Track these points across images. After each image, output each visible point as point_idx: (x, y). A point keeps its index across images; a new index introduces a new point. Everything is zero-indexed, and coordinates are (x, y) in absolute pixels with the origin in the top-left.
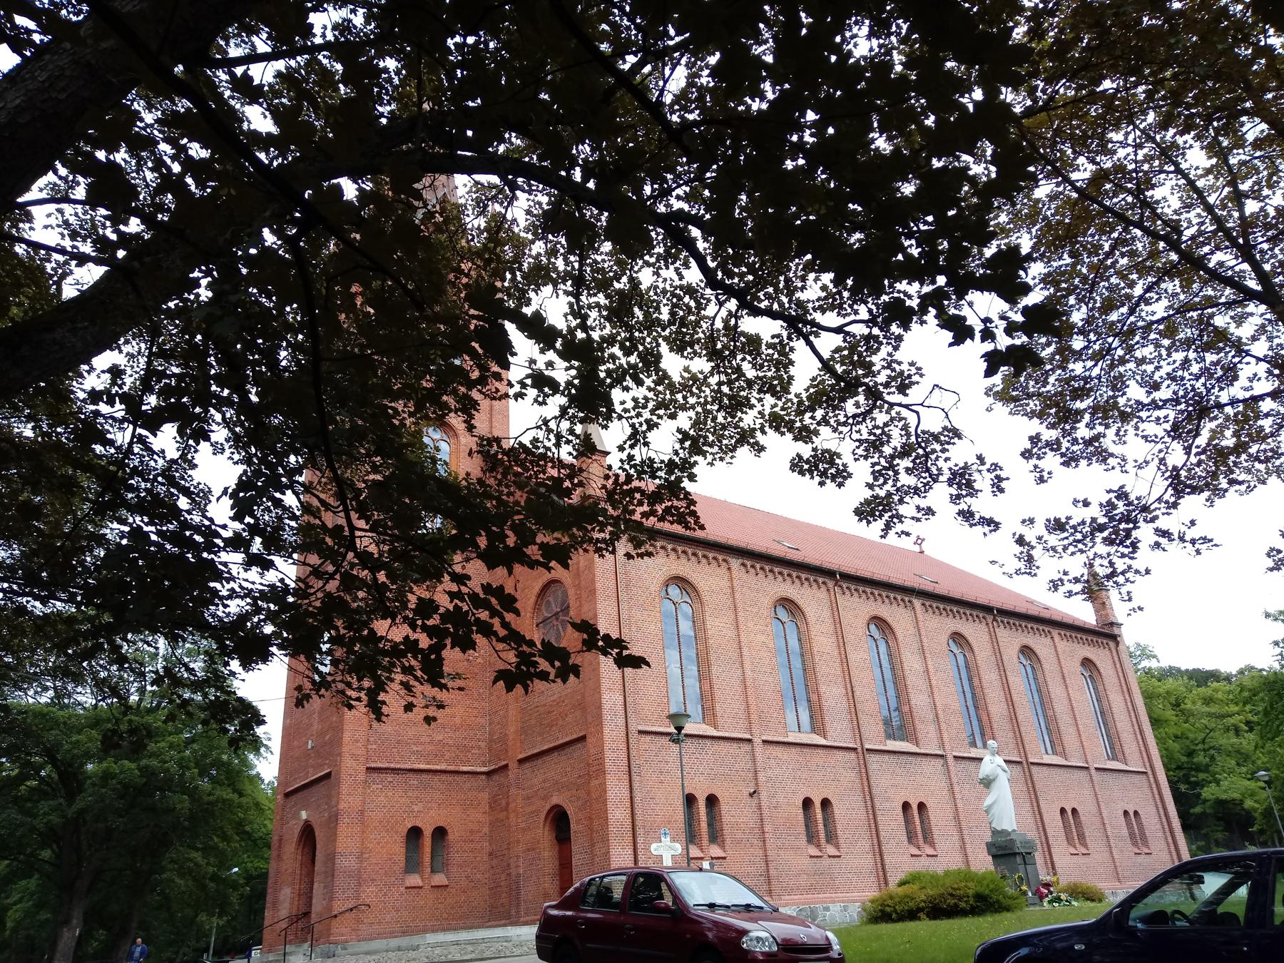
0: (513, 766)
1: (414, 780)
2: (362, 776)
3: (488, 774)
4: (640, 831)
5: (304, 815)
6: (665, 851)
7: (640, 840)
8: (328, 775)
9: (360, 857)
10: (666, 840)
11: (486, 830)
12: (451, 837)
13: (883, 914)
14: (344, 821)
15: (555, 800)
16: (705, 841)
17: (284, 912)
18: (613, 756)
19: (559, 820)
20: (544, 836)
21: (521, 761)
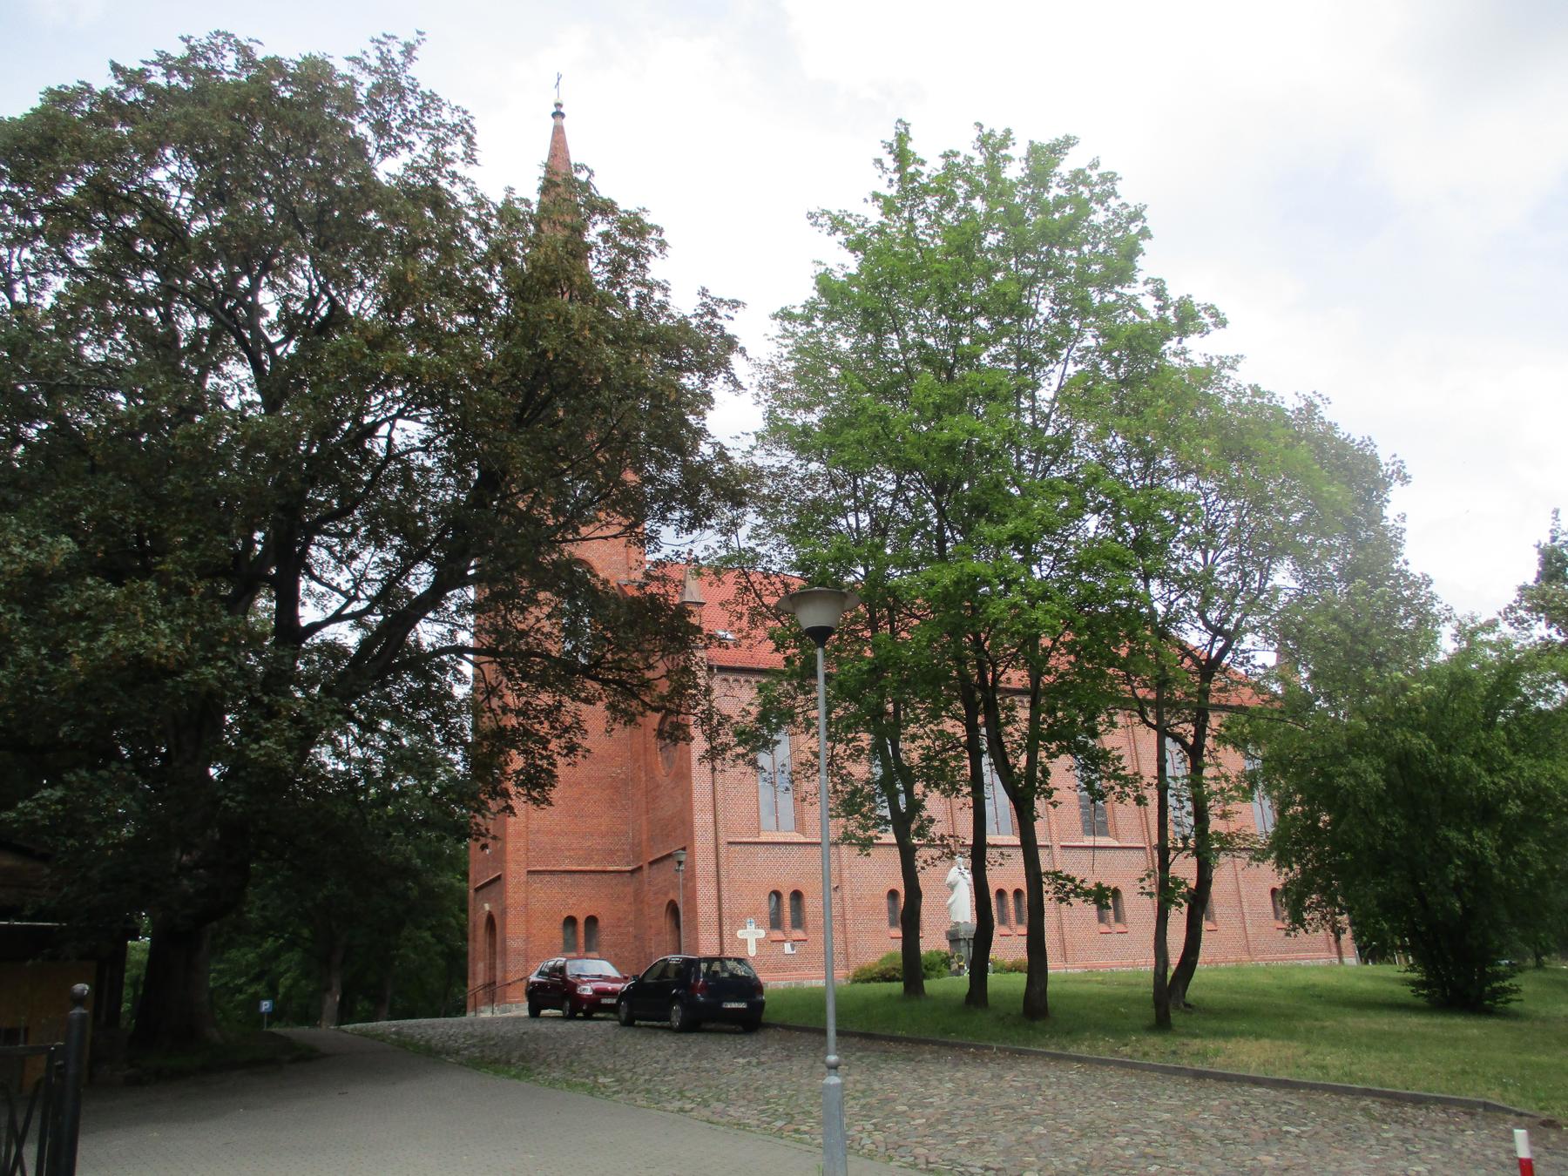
0: (646, 867)
1: (568, 879)
2: (524, 878)
3: (632, 872)
4: (725, 921)
5: (487, 907)
6: (751, 938)
7: (726, 928)
8: (499, 877)
9: (527, 940)
10: (751, 928)
11: (631, 917)
12: (601, 924)
13: (857, 979)
14: (511, 913)
15: (671, 896)
16: (788, 928)
17: (480, 981)
18: (703, 862)
19: (673, 909)
20: (664, 922)
21: (651, 863)
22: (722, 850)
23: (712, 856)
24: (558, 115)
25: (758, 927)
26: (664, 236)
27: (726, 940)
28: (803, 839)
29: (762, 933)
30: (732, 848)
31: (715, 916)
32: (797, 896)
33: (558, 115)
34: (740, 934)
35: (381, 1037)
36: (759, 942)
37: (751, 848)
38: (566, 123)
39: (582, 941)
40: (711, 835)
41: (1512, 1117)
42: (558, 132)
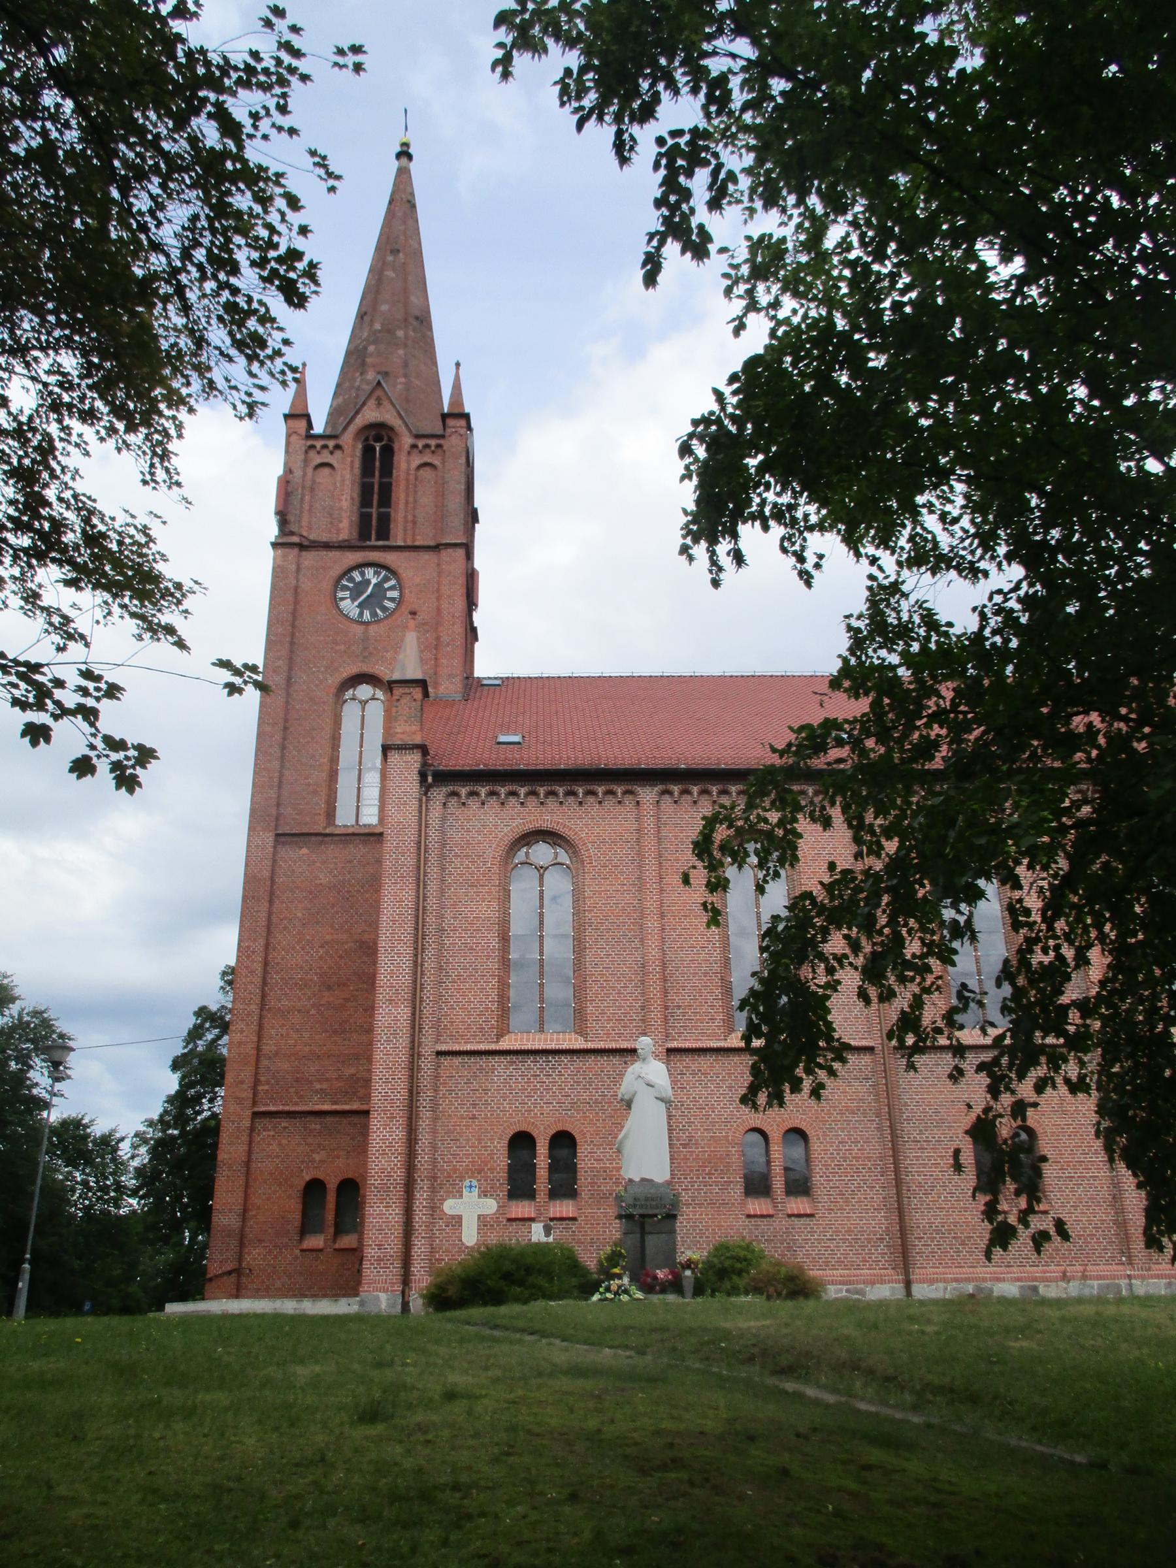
1: (315, 1125)
7: (421, 1197)
16: (542, 1196)
22: (427, 1065)
23: (402, 1075)
24: (404, 154)
25: (484, 1194)
26: (722, 576)
27: (420, 1217)
28: (579, 1043)
29: (490, 1206)
30: (446, 1061)
31: (399, 1175)
32: (563, 1141)
33: (404, 154)
34: (450, 1206)
35: (207, 1320)
36: (484, 1222)
37: (482, 1062)
38: (413, 166)
39: (330, 1216)
40: (403, 1041)
41: (276, 764)
42: (403, 178)
